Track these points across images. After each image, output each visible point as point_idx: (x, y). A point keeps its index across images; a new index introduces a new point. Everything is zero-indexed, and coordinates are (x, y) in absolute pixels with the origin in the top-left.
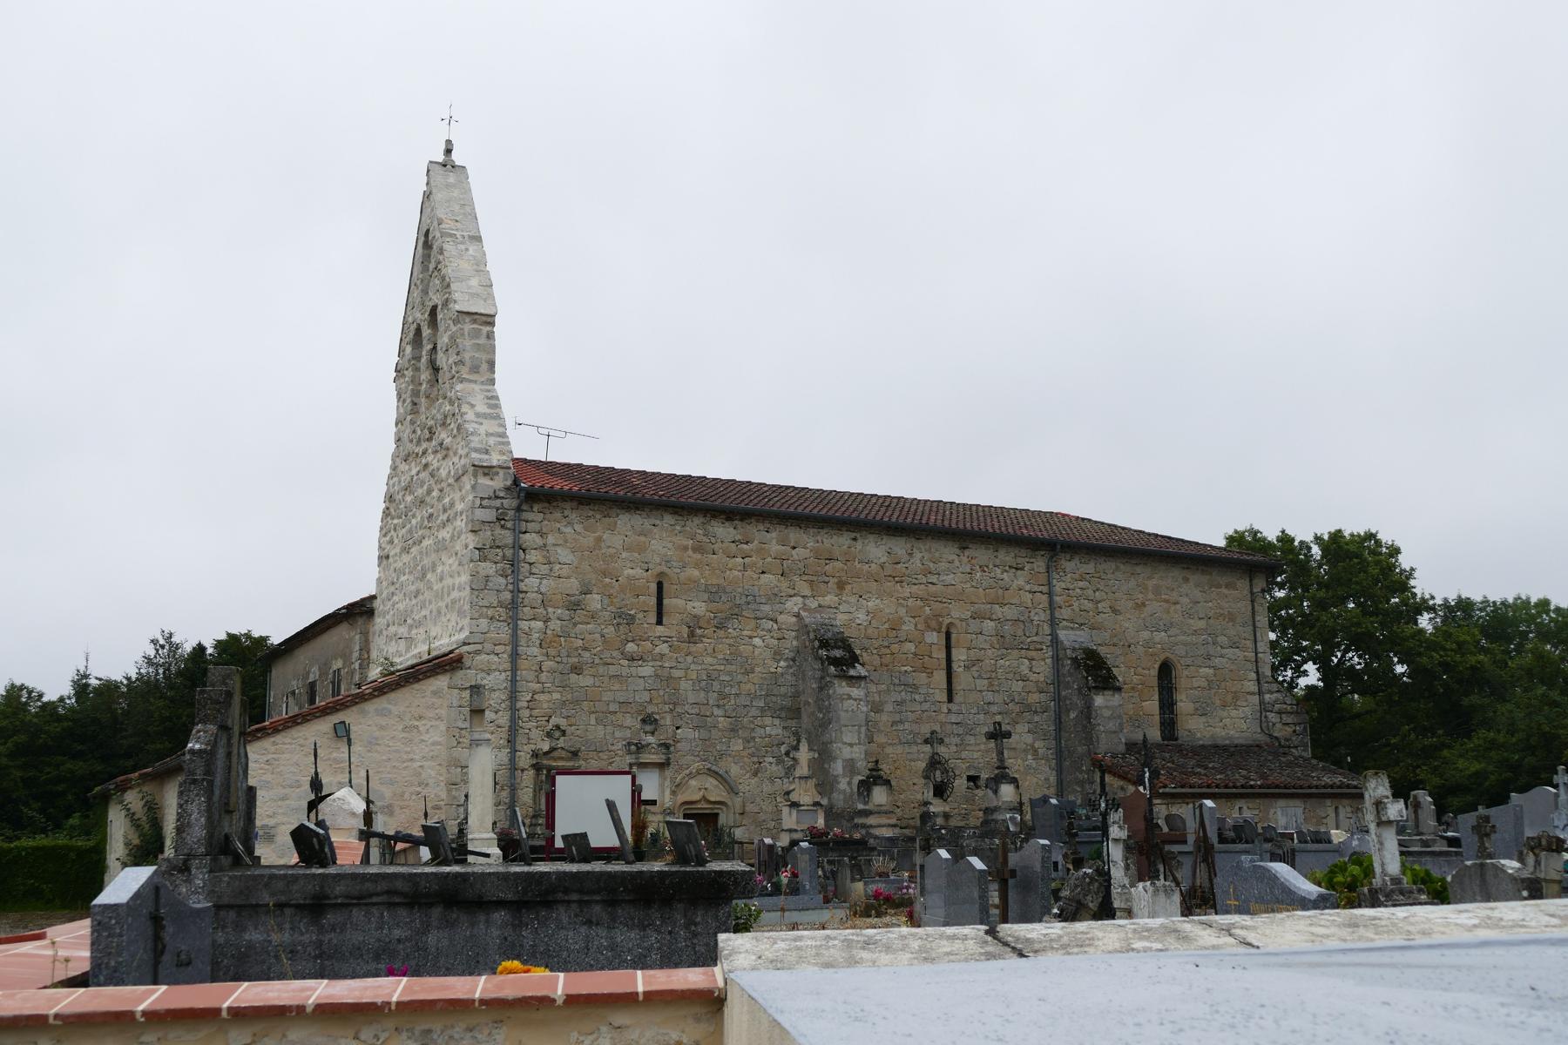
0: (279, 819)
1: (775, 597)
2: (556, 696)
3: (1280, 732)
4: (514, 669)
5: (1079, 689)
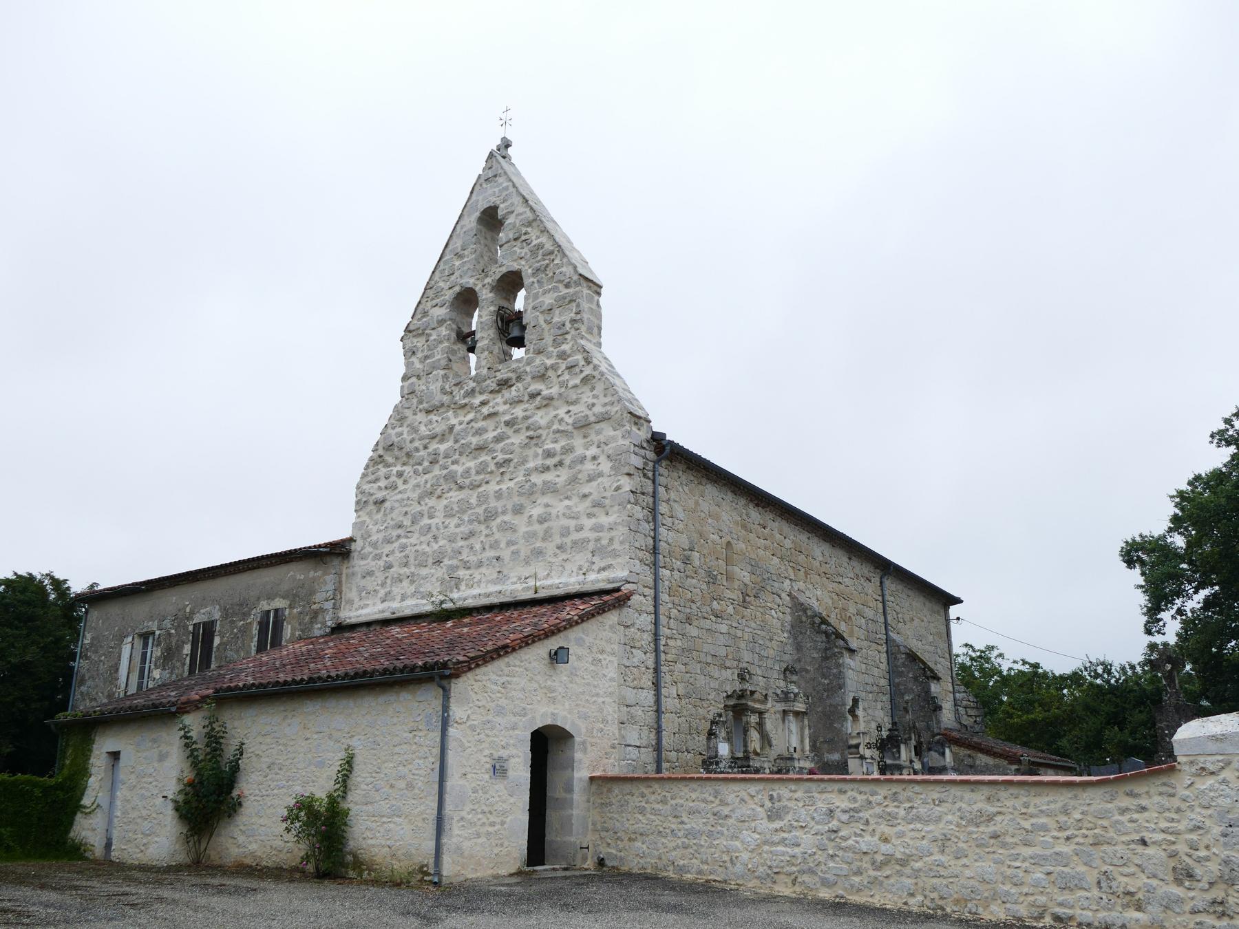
0: (513, 751)
1: (781, 577)
2: (679, 643)
3: (966, 721)
4: (656, 613)
5: (915, 679)
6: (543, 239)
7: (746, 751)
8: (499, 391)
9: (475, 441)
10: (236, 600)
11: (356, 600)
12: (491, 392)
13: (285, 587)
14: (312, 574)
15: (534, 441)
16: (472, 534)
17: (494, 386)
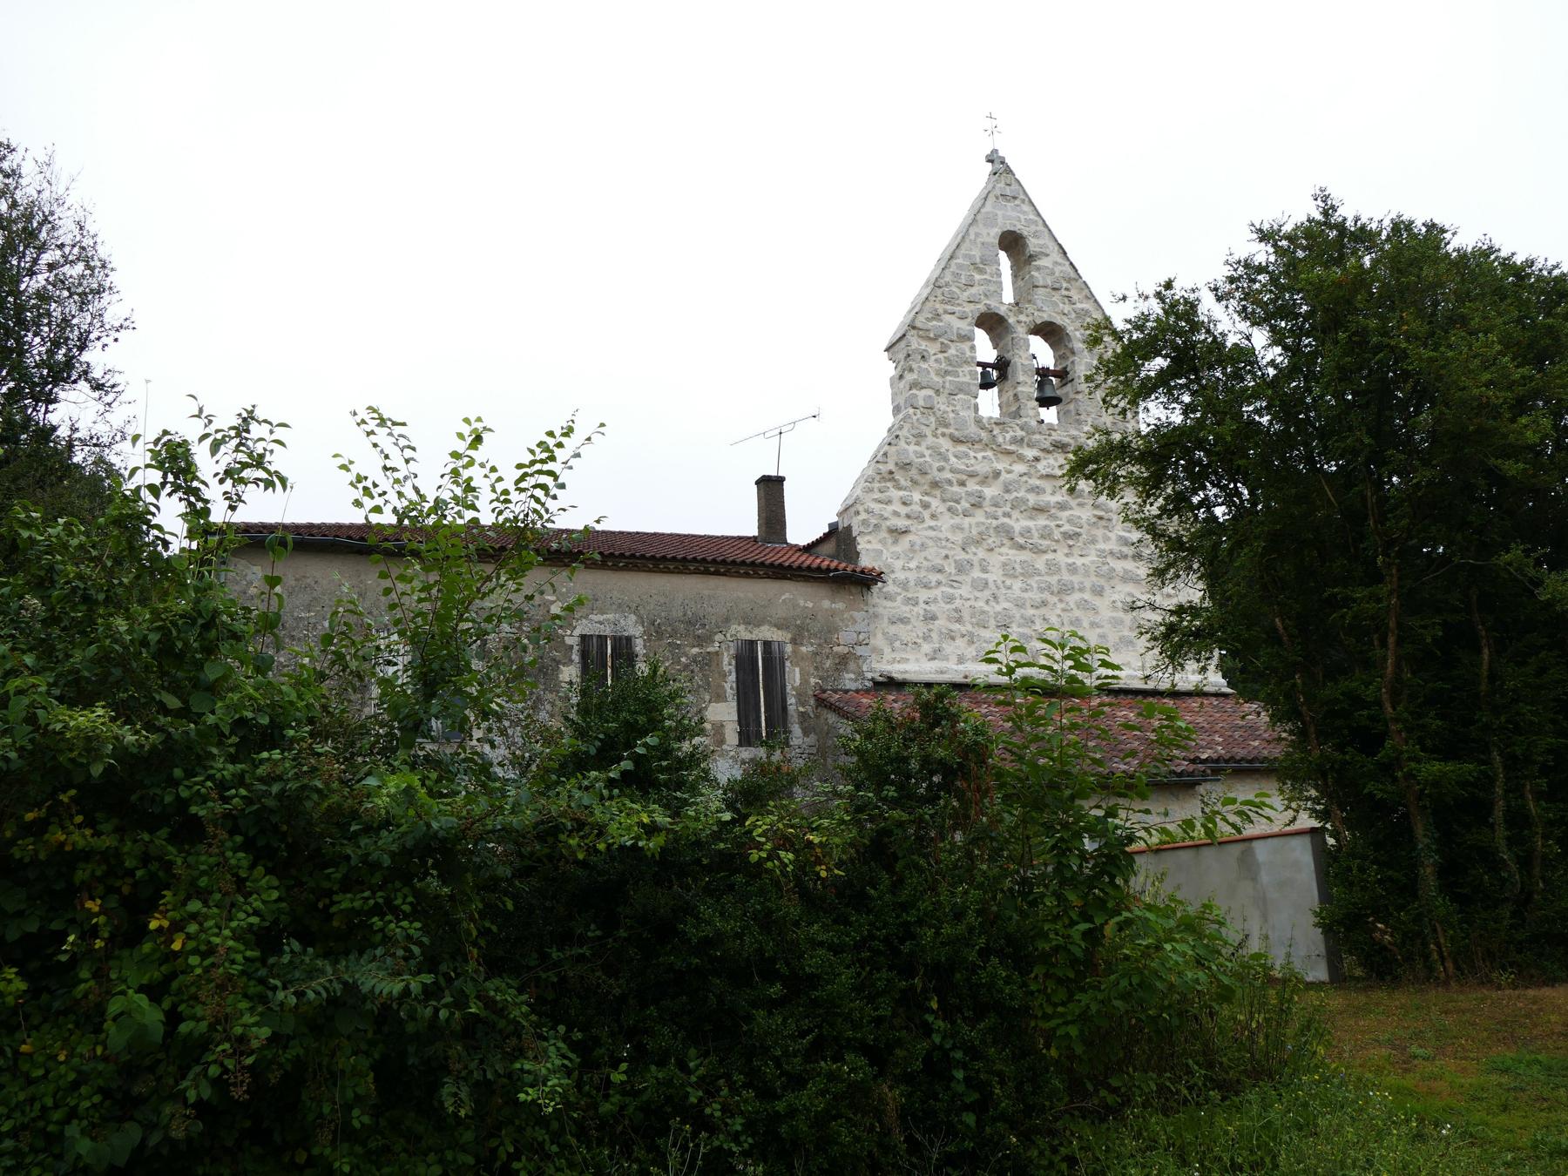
6: (1087, 306)
7: (1072, 798)
8: (1049, 452)
9: (1032, 499)
10: (677, 613)
11: (887, 650)
12: (1043, 450)
13: (780, 612)
14: (826, 604)
15: (1103, 523)
16: (1044, 603)
17: (1047, 445)
